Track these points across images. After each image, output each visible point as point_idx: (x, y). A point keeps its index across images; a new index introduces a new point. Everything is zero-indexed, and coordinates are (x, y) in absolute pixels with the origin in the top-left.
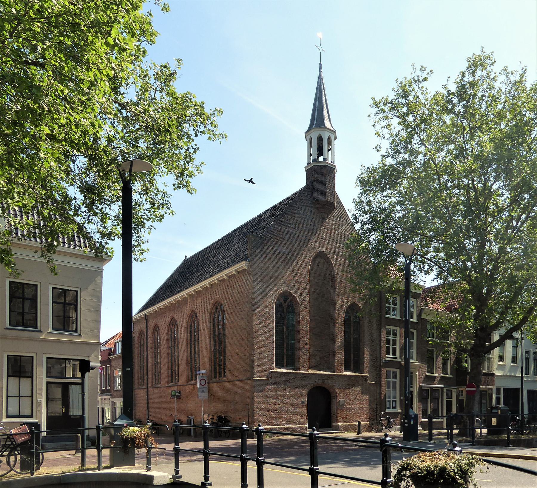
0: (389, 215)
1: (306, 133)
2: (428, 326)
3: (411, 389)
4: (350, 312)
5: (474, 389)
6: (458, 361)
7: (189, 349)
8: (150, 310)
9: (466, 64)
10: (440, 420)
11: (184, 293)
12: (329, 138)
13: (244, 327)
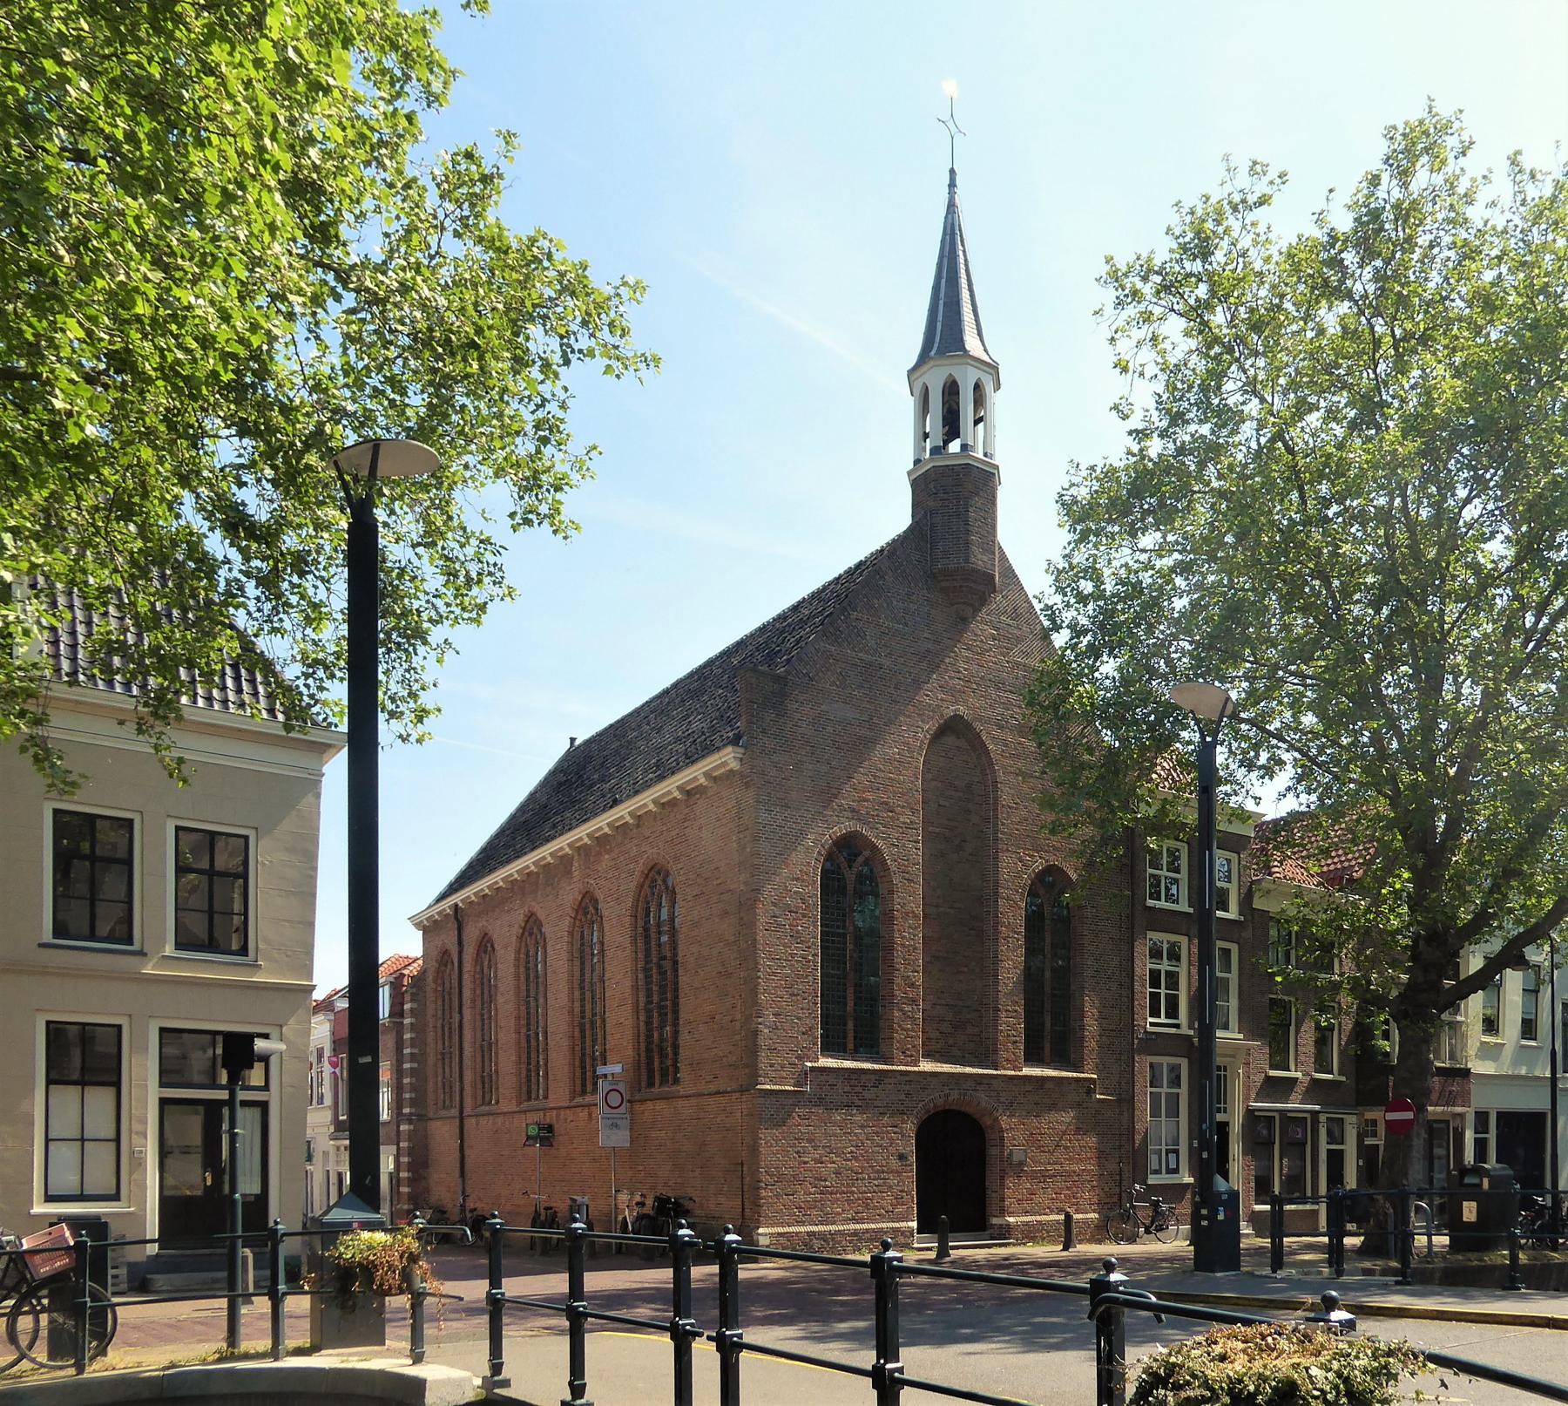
0: (1154, 604)
1: (911, 372)
2: (1273, 933)
3: (1220, 1117)
4: (1042, 891)
5: (1409, 1115)
6: (1362, 1033)
7: (577, 1004)
8: (469, 892)
9: (1383, 148)
10: (1308, 1207)
11: (562, 843)
12: (978, 387)
13: (732, 939)
